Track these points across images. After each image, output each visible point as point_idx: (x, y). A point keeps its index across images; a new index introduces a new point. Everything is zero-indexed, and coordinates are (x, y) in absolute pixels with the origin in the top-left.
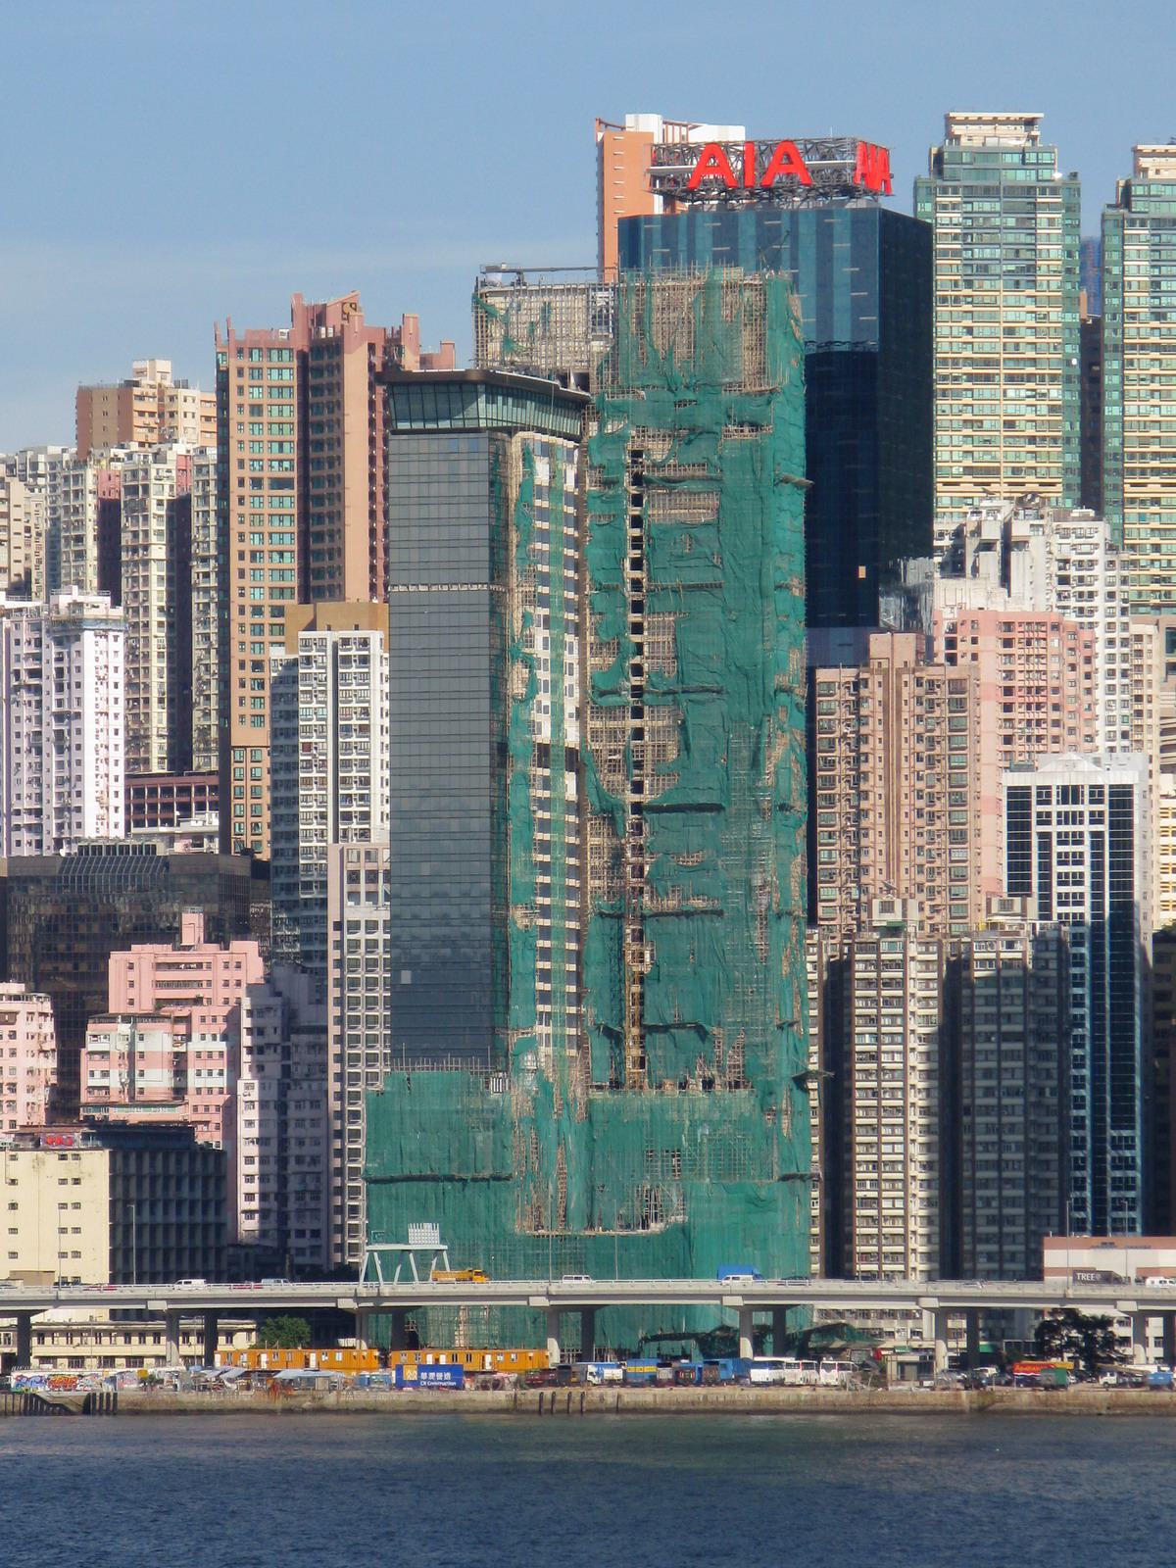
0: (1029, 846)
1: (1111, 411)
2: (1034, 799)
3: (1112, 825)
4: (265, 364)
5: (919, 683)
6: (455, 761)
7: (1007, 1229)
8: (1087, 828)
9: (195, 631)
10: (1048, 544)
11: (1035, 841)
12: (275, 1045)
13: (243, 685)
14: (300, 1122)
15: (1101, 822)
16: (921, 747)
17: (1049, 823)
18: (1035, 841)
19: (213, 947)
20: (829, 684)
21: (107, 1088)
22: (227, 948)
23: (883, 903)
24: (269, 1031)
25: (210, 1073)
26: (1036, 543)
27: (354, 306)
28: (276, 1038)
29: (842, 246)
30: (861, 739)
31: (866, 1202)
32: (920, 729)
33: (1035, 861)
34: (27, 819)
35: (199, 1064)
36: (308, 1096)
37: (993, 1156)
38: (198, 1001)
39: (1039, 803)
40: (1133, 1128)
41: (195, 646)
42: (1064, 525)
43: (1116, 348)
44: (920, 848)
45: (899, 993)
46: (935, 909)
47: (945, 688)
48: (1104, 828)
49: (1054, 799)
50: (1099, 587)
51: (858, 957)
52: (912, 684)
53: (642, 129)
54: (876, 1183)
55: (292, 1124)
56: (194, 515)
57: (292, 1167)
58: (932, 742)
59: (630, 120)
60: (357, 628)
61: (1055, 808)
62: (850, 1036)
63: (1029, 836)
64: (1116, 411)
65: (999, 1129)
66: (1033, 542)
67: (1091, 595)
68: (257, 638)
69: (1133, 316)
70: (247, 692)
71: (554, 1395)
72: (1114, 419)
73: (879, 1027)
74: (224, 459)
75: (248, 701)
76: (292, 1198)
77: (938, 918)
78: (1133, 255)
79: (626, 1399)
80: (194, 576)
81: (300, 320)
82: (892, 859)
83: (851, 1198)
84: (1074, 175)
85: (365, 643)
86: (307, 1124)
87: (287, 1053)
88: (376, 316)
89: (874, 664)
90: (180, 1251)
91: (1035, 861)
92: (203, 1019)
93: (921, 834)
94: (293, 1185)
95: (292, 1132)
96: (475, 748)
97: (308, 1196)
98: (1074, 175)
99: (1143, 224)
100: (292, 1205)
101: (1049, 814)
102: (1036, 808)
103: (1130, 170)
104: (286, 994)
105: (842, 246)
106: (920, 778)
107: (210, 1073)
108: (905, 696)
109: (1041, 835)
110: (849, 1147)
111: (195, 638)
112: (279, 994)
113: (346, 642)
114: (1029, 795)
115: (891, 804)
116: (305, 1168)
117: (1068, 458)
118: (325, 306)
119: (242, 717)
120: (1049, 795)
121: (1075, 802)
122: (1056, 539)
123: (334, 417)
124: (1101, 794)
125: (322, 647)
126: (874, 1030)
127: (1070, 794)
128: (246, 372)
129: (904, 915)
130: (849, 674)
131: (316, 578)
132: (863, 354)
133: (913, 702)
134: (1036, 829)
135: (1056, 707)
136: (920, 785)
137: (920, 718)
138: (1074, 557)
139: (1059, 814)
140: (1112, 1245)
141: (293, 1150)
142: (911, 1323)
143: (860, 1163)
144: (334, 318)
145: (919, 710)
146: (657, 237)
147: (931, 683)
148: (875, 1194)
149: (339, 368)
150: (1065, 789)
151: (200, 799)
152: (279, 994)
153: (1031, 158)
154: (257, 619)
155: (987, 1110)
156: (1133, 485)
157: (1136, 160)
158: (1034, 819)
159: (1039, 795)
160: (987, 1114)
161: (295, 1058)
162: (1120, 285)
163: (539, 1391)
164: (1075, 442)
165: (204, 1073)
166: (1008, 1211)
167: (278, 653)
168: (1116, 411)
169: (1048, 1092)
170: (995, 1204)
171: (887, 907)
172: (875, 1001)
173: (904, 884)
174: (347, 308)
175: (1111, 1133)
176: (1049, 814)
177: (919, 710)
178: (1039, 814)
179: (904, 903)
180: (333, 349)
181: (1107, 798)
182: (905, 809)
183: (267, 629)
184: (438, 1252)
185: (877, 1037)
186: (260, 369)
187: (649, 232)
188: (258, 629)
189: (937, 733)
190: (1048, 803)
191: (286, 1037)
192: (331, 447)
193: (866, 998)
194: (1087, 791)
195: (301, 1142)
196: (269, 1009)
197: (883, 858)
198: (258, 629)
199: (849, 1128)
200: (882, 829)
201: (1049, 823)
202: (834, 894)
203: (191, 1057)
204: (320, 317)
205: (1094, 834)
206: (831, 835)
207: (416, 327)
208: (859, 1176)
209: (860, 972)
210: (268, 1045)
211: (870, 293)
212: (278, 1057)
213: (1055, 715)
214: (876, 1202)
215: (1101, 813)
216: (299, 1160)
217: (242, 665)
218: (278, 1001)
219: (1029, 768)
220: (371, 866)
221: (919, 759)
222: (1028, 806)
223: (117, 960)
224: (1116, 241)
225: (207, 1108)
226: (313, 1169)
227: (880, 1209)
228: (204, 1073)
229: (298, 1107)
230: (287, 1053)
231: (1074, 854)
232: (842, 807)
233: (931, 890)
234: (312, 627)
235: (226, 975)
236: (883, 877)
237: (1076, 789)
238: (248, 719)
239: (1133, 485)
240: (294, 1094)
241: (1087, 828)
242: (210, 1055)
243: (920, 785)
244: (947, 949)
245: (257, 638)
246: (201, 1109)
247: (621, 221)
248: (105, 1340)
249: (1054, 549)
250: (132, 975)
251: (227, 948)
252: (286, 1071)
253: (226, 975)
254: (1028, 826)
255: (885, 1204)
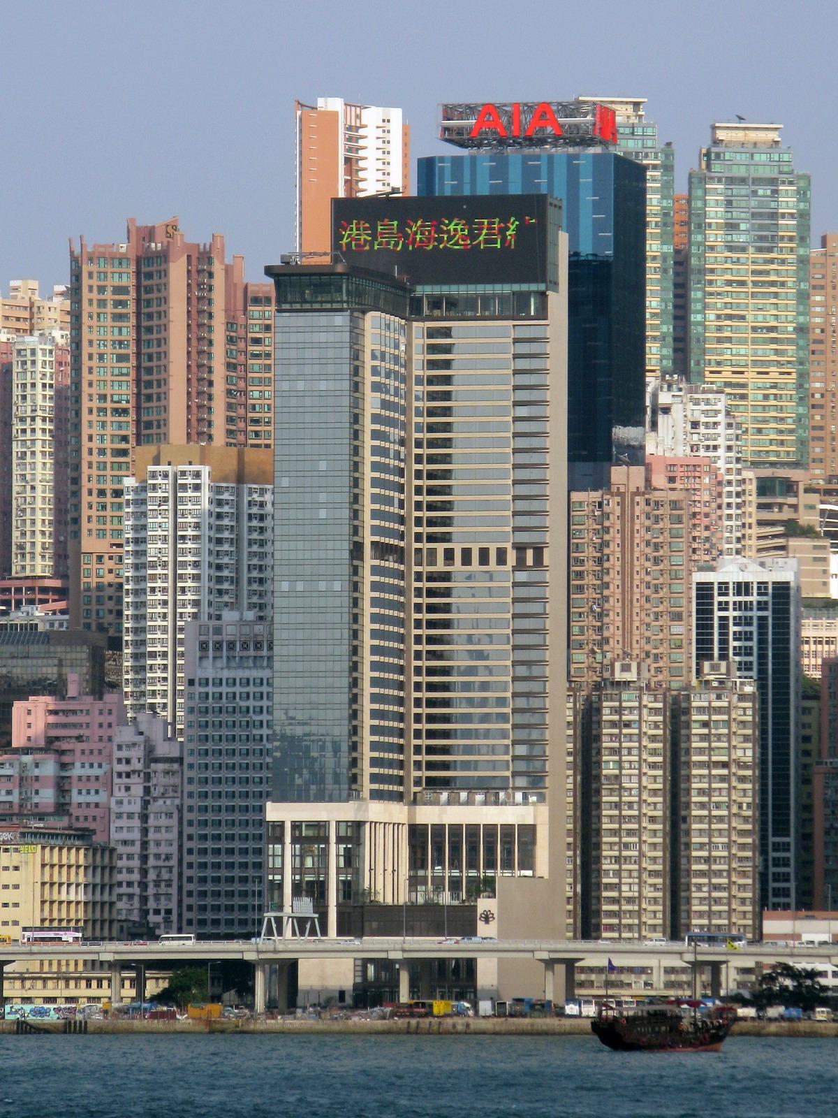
0: (712, 627)
1: (696, 318)
2: (716, 592)
3: (774, 611)
4: (109, 269)
5: (648, 503)
6: (323, 555)
7: (715, 908)
8: (755, 614)
9: (14, 472)
10: (685, 410)
11: (716, 623)
12: (139, 772)
13: (91, 507)
14: (158, 829)
15: (766, 609)
16: (648, 550)
17: (727, 610)
18: (716, 623)
19: (89, 699)
20: (581, 503)
21: (11, 803)
22: (101, 699)
23: (623, 666)
24: (134, 761)
25: (88, 792)
26: (677, 411)
27: (175, 228)
28: (139, 766)
29: (586, 180)
30: (605, 544)
31: (610, 887)
32: (648, 537)
33: (716, 637)
34: (190, 571)
35: (81, 785)
36: (164, 809)
37: (705, 854)
38: (79, 738)
39: (720, 595)
40: (788, 835)
41: (14, 483)
42: (696, 396)
43: (699, 272)
44: (648, 625)
45: (725, 717)
46: (659, 670)
47: (667, 506)
48: (768, 613)
49: (731, 592)
50: (721, 441)
51: (605, 704)
52: (643, 503)
53: (330, 109)
54: (618, 873)
55: (152, 830)
56: (14, 386)
57: (152, 862)
58: (657, 547)
59: (321, 103)
60: (190, 463)
61: (731, 598)
62: (599, 763)
63: (712, 619)
64: (699, 317)
65: (710, 833)
66: (674, 409)
67: (715, 448)
68: (102, 473)
69: (712, 248)
70: (94, 513)
71: (418, 1023)
72: (698, 323)
73: (620, 756)
74: (76, 342)
75: (94, 519)
76: (151, 885)
77: (660, 677)
78: (712, 203)
79: (472, 1027)
80: (14, 432)
81: (134, 239)
82: (626, 630)
83: (598, 885)
84: (669, 144)
85: (197, 475)
86: (163, 830)
87: (148, 777)
88: (194, 234)
89: (614, 489)
90: (103, 922)
91: (716, 637)
92: (83, 752)
93: (648, 615)
94: (152, 875)
95: (152, 835)
96: (338, 545)
97: (163, 884)
98: (669, 144)
99: (720, 181)
100: (151, 890)
101: (727, 603)
102: (717, 599)
103: (709, 142)
104: (146, 733)
105: (586, 180)
106: (648, 573)
107: (88, 792)
108: (637, 512)
109: (721, 618)
110: (598, 846)
111: (14, 477)
112: (141, 733)
113: (183, 473)
114: (712, 589)
115: (626, 588)
116: (161, 863)
117: (665, 352)
118: (153, 227)
119: (90, 530)
120: (727, 588)
121: (747, 594)
122: (691, 406)
123: (162, 309)
124: (766, 588)
125: (166, 476)
126: (617, 758)
127: (742, 588)
128: (95, 275)
129: (639, 674)
130: (595, 496)
131: (146, 428)
132: (602, 262)
133: (643, 517)
134: (717, 614)
135: (707, 528)
136: (648, 578)
137: (648, 529)
138: (703, 419)
139: (735, 603)
140: (813, 917)
141: (152, 849)
142: (644, 977)
143: (606, 857)
144: (160, 235)
145: (648, 523)
146: (448, 173)
147: (657, 503)
148: (616, 881)
149: (166, 273)
150: (739, 584)
151: (18, 597)
152: (141, 733)
153: (639, 131)
154: (102, 458)
155: (700, 819)
156: (712, 372)
157: (714, 134)
158: (716, 607)
159: (720, 589)
160: (701, 822)
161: (154, 781)
162: (702, 227)
163: (407, 1020)
164: (670, 340)
165: (84, 792)
166: (715, 894)
167: (130, 482)
168: (699, 317)
169: (745, 806)
170: (705, 889)
171: (626, 668)
172: (618, 736)
173: (635, 652)
174: (170, 229)
175: (771, 839)
176: (727, 603)
177: (648, 523)
178: (720, 603)
179: (639, 665)
180: (164, 257)
181: (770, 591)
182: (637, 596)
183: (109, 466)
184: (312, 919)
185: (620, 764)
186: (105, 273)
187: (442, 169)
188: (102, 466)
189: (661, 540)
190: (727, 595)
191: (147, 766)
192: (159, 332)
193: (611, 735)
194: (755, 586)
195: (158, 844)
196: (134, 744)
197: (620, 632)
198: (102, 466)
199: (598, 832)
200: (619, 610)
201: (727, 609)
202: (582, 658)
203: (75, 781)
204: (150, 234)
205: (760, 618)
206: (580, 614)
207: (223, 245)
208: (604, 867)
209: (607, 716)
210: (134, 772)
211: (607, 216)
212: (141, 780)
213: (707, 534)
214: (617, 887)
215: (766, 603)
216: (157, 856)
217: (90, 493)
218: (141, 738)
219: (712, 569)
220: (217, 638)
221: (648, 559)
222: (712, 597)
223: (18, 708)
224: (700, 193)
225: (86, 818)
226: (167, 864)
227: (620, 891)
228: (84, 792)
229: (156, 818)
230: (148, 777)
231: (746, 633)
232: (590, 594)
233: (656, 656)
234: (157, 461)
235: (101, 719)
236: (620, 646)
237: (747, 584)
238: (94, 533)
239: (712, 372)
240: (153, 807)
241: (755, 614)
242: (88, 778)
243: (648, 578)
244: (670, 700)
245: (102, 473)
246: (81, 819)
247: (420, 161)
248: (50, 984)
249: (689, 413)
250: (30, 719)
251: (101, 699)
252: (147, 790)
253: (101, 719)
254: (712, 612)
255: (624, 888)
